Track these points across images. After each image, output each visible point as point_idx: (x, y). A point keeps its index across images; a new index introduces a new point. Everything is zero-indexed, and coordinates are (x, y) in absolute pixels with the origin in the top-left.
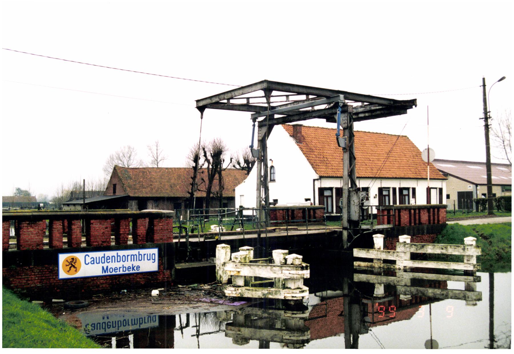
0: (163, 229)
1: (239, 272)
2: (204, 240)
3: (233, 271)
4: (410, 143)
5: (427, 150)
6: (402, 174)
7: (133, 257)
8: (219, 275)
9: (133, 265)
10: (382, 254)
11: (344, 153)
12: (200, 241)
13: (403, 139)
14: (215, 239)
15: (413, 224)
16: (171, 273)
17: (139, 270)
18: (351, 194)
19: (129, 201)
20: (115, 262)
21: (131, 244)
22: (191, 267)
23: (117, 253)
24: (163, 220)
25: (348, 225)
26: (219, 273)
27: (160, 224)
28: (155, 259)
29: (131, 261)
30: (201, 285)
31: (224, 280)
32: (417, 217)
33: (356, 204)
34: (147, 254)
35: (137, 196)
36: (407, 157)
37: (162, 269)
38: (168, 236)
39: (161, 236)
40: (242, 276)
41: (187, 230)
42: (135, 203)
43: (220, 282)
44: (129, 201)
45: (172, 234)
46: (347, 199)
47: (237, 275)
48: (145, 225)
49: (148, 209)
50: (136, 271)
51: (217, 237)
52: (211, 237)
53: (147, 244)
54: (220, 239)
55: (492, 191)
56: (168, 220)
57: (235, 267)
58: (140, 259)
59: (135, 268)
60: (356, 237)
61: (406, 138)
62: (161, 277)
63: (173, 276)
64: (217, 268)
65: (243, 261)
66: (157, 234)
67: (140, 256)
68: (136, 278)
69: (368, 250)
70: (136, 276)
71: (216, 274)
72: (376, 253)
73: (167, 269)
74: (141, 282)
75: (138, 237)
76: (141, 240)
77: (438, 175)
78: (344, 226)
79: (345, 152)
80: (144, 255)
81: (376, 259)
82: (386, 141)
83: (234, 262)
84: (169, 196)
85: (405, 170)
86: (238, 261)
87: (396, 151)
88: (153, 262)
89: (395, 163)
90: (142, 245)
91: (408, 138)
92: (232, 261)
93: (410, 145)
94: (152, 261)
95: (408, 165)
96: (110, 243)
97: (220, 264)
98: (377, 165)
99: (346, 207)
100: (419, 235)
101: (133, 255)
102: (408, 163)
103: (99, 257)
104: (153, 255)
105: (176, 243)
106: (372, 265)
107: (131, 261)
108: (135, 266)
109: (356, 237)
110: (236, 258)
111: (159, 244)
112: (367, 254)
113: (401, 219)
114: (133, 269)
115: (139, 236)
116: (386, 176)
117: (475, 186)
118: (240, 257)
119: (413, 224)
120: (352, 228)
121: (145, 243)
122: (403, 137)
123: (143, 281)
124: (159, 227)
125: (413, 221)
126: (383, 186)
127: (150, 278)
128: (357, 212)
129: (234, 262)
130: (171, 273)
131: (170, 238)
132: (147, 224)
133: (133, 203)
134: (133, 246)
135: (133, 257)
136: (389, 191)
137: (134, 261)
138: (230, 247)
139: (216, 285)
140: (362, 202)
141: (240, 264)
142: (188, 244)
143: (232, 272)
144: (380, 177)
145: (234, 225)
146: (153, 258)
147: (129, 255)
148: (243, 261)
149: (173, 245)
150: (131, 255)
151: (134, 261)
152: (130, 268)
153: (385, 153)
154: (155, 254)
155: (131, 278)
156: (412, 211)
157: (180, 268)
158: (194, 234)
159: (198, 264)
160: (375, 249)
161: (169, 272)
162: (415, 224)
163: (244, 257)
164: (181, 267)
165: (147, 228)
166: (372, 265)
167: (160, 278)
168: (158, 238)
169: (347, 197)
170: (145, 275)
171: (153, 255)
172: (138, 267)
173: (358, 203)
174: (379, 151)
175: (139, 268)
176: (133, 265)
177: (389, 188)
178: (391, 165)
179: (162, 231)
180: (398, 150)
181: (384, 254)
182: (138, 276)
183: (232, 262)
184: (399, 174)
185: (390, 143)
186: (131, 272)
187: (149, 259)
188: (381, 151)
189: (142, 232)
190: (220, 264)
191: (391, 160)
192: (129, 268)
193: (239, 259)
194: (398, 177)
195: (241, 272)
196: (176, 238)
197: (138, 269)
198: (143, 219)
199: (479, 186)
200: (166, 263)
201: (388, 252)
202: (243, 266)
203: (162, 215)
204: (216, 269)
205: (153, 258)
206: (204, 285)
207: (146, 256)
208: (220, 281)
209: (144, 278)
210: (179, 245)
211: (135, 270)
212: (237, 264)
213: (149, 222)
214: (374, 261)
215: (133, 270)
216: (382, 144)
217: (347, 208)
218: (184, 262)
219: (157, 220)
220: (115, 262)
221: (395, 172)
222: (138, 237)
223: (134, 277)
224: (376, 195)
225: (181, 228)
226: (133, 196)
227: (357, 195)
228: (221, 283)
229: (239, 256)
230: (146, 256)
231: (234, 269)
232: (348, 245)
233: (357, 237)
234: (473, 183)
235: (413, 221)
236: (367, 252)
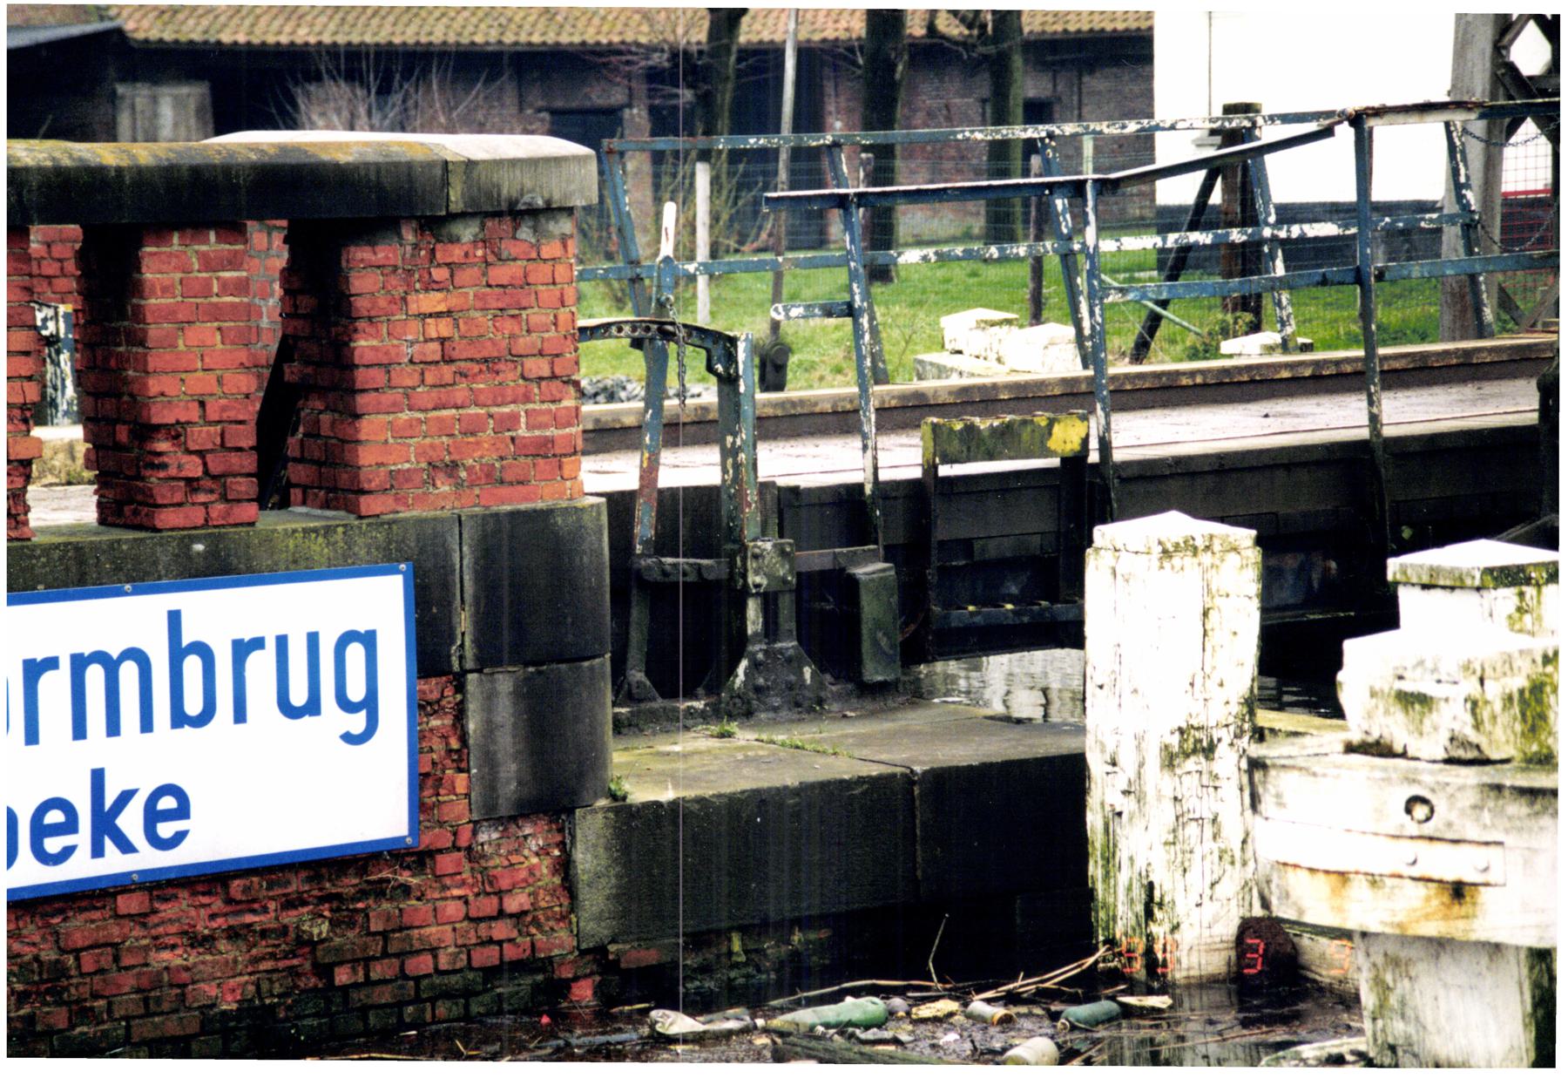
0: (460, 350)
1: (1458, 891)
2: (930, 469)
3: (1374, 881)
7: (95, 676)
8: (1123, 878)
9: (98, 777)
12: (884, 476)
14: (1048, 453)
16: (565, 866)
17: (180, 837)
19: (121, 89)
20: (147, 725)
21: (73, 530)
22: (789, 777)
23: (174, 618)
24: (456, 253)
26: (1123, 854)
27: (432, 301)
28: (370, 704)
29: (79, 731)
30: (926, 1011)
31: (1186, 936)
34: (282, 642)
35: (197, 37)
37: (457, 809)
38: (522, 432)
39: (444, 429)
40: (1495, 949)
41: (731, 358)
42: (178, 103)
43: (1138, 968)
44: (121, 89)
45: (569, 403)
47: (1431, 929)
48: (250, 312)
50: (148, 859)
51: (1067, 435)
52: (1006, 432)
53: (272, 522)
54: (1105, 446)
55: (1351, 204)
56: (508, 248)
57: (1413, 829)
58: (193, 706)
59: (131, 821)
62: (453, 909)
63: (595, 900)
64: (1103, 793)
65: (1502, 740)
66: (395, 408)
67: (192, 667)
68: (136, 936)
70: (140, 919)
71: (1095, 870)
73: (527, 809)
74: (210, 990)
75: (163, 446)
76: (192, 484)
80: (242, 650)
83: (1379, 749)
84: (509, 38)
86: (1435, 746)
88: (348, 738)
90: (214, 542)
92: (1356, 737)
94: (333, 719)
96: (672, 199)
97: (1139, 739)
101: (100, 657)
103: (313, 640)
104: (355, 652)
105: (620, 504)
107: (79, 731)
108: (126, 797)
110: (1414, 701)
111: (420, 522)
114: (105, 826)
115: (176, 432)
118: (1470, 687)
121: (250, 510)
123: (232, 969)
124: (413, 330)
127: (321, 929)
129: (1379, 749)
130: (565, 866)
131: (543, 450)
132: (270, 307)
133: (167, 112)
134: (95, 547)
135: (95, 676)
137: (113, 728)
138: (1259, 541)
139: (1103, 1007)
141: (1470, 775)
142: (751, 515)
143: (1359, 886)
145: (1164, 304)
146: (356, 692)
147: (52, 663)
148: (1502, 740)
149: (578, 532)
150: (79, 664)
151: (113, 728)
152: (70, 826)
154: (368, 640)
155: (79, 940)
157: (667, 795)
158: (791, 393)
159: (863, 741)
161: (542, 852)
163: (1518, 682)
164: (674, 778)
165: (268, 346)
167: (432, 930)
168: (408, 460)
170: (251, 904)
171: (355, 652)
172: (167, 803)
175: (183, 812)
176: (98, 777)
179: (447, 372)
182: (168, 910)
183: (1350, 749)
186: (82, 867)
187: (298, 697)
189: (200, 382)
190: (1139, 739)
192: (55, 817)
193: (1451, 718)
195: (1485, 895)
196: (607, 438)
197: (166, 830)
198: (212, 244)
200: (506, 742)
202: (1518, 808)
203: (446, 183)
204: (1093, 801)
205: (356, 692)
206: (963, 998)
207: (261, 666)
208: (1149, 952)
209: (233, 934)
210: (644, 527)
211: (126, 847)
212: (1430, 778)
213: (287, 275)
215: (98, 851)
218: (704, 716)
219: (384, 252)
220: (147, 725)
222: (163, 446)
223: (115, 931)
225: (668, 336)
226: (154, 35)
228: (1156, 974)
229: (1449, 668)
230: (261, 666)
231: (1394, 857)
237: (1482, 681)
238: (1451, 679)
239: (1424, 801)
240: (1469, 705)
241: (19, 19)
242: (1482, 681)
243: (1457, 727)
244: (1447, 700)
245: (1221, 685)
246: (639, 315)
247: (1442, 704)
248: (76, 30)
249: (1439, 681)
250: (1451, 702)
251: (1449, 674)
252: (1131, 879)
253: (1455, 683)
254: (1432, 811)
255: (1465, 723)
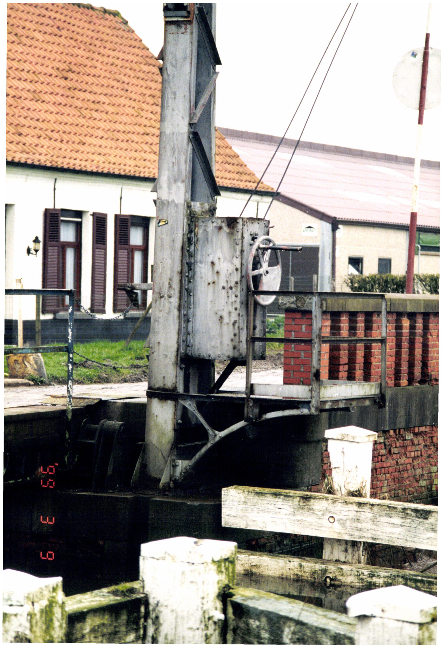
4: (134, 43)
5: (420, 57)
6: (129, 162)
10: (385, 519)
11: (173, 28)
13: (108, 23)
15: (404, 382)
18: (200, 231)
25: (181, 374)
32: (418, 351)
33: (222, 283)
36: (133, 96)
46: (178, 254)
49: (408, 292)
60: (222, 434)
61: (117, 18)
69: (307, 499)
72: (352, 515)
77: (245, 177)
78: (158, 384)
79: (178, 24)
81: (339, 541)
82: (50, 22)
85: (134, 145)
87: (93, 71)
89: (95, 115)
91: (125, 23)
93: (136, 51)
95: (141, 130)
98: (31, 114)
99: (176, 293)
100: (423, 429)
102: (138, 120)
106: (325, 571)
109: (222, 434)
112: (299, 517)
113: (372, 359)
116: (72, 161)
117: (328, 226)
118: (28, 608)
119: (404, 382)
120: (193, 392)
122: (107, 16)
125: (404, 368)
126: (58, 207)
128: (226, 320)
136: (79, 227)
140: (256, 272)
144: (55, 165)
153: (54, 73)
156: (406, 323)
160: (330, 491)
162: (411, 381)
166: (325, 571)
169: (179, 244)
173: (237, 277)
174: (34, 60)
177: (79, 214)
178: (82, 121)
180: (99, 65)
181: (397, 520)
184: (118, 160)
185: (64, 33)
188: (40, 60)
191: (79, 104)
194: (117, 172)
199: (340, 226)
201: (416, 511)
214: (327, 553)
216: (37, 35)
217: (180, 298)
221: (102, 151)
224: (36, 240)
227: (231, 234)
232: (178, 470)
233: (223, 439)
234: (322, 216)
235: (404, 368)
236: (302, 508)
237: (33, 603)
238: (19, 604)
239: (332, 517)
240: (29, 618)
241: (215, 4)
242: (33, 603)
243: (20, 630)
244: (16, 615)
245: (190, 552)
246: (199, 392)
247: (13, 617)
248: (212, 108)
249: (11, 605)
250: (19, 616)
251: (18, 602)
252: (181, 69)
253: (22, 606)
254: (330, 517)
255: (26, 628)
